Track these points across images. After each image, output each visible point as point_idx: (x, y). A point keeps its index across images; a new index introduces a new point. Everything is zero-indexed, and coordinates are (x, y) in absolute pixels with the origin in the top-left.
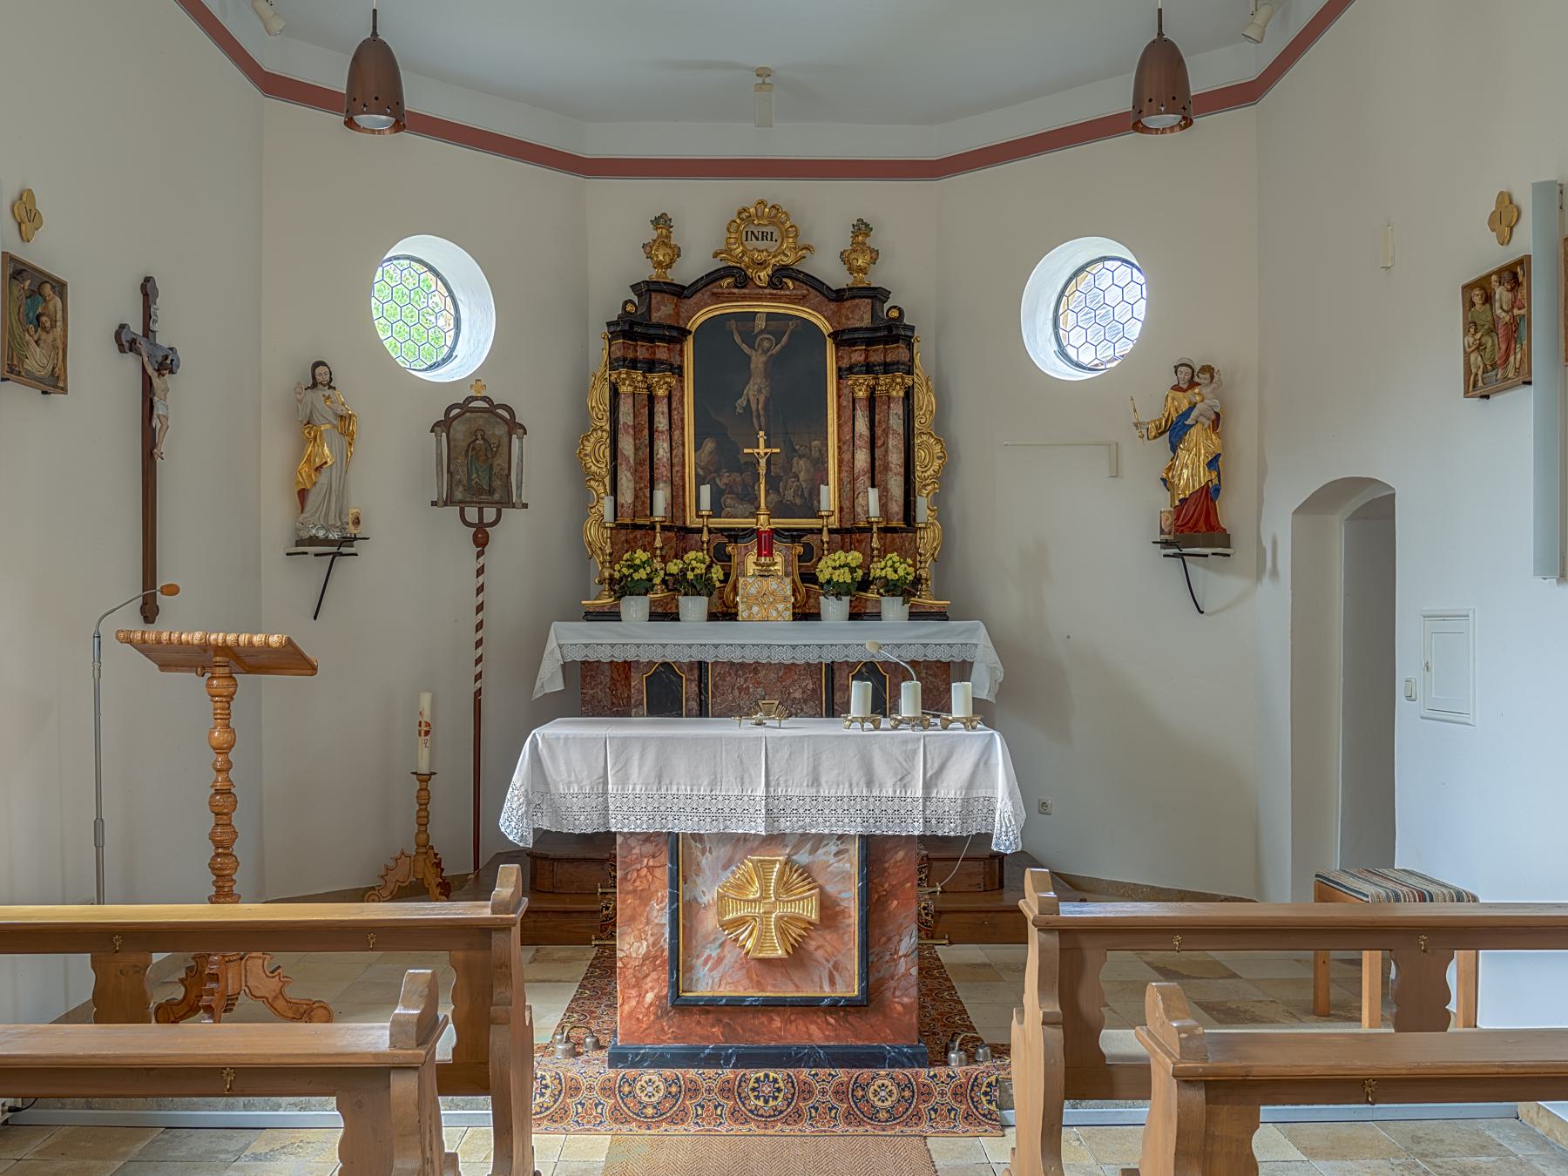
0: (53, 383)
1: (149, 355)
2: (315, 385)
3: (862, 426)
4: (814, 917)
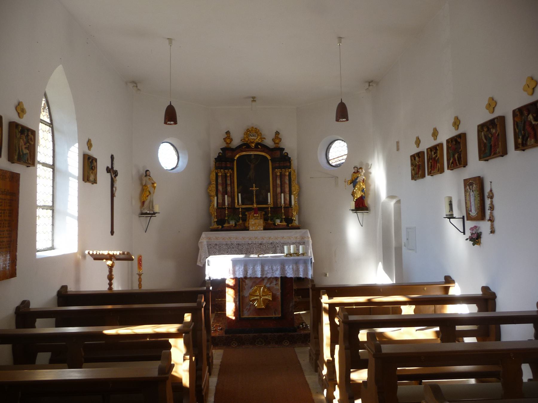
0: (95, 182)
1: (111, 171)
2: (146, 176)
3: (278, 182)
4: (270, 299)
